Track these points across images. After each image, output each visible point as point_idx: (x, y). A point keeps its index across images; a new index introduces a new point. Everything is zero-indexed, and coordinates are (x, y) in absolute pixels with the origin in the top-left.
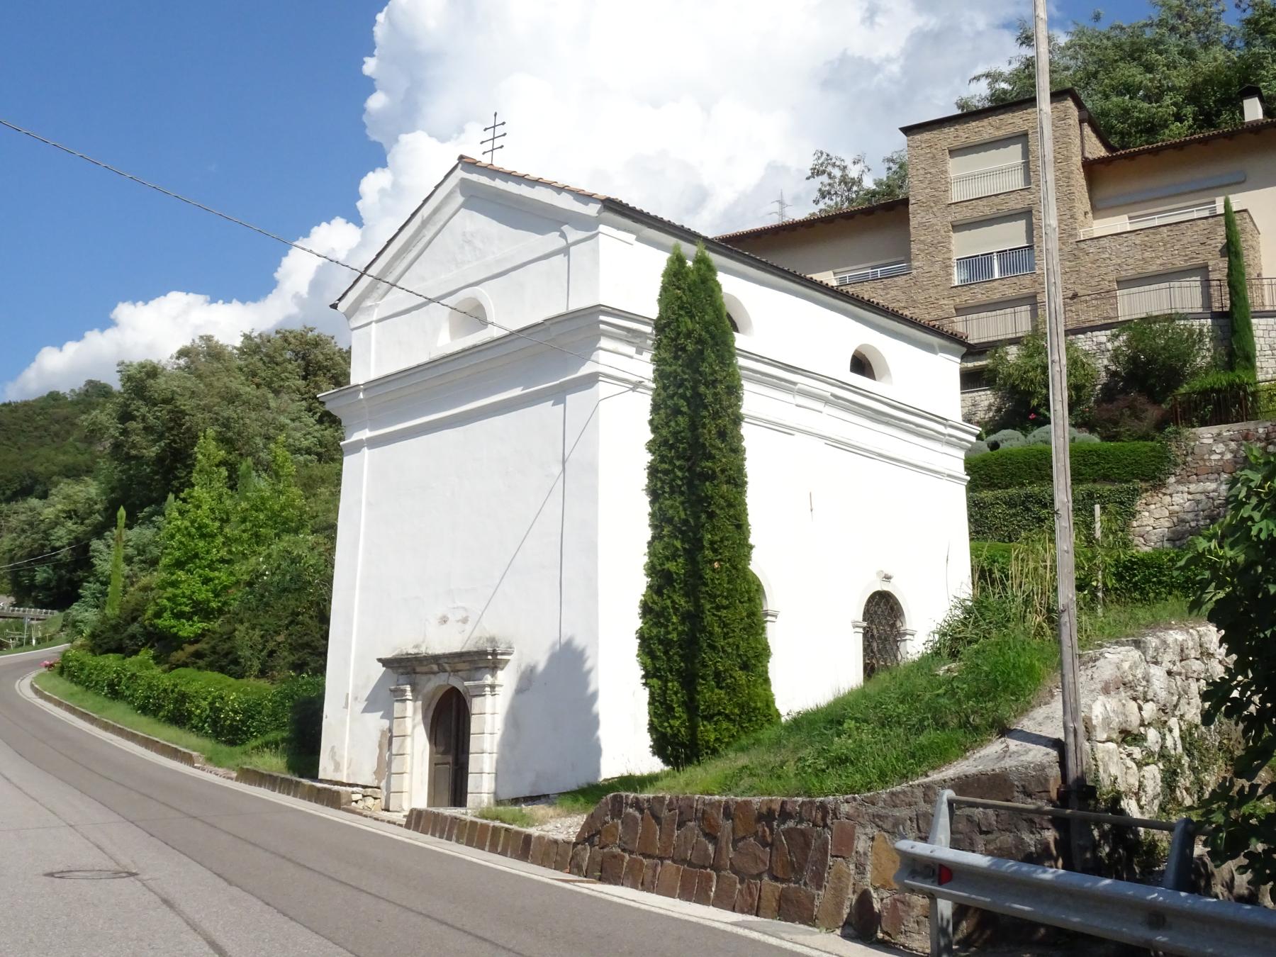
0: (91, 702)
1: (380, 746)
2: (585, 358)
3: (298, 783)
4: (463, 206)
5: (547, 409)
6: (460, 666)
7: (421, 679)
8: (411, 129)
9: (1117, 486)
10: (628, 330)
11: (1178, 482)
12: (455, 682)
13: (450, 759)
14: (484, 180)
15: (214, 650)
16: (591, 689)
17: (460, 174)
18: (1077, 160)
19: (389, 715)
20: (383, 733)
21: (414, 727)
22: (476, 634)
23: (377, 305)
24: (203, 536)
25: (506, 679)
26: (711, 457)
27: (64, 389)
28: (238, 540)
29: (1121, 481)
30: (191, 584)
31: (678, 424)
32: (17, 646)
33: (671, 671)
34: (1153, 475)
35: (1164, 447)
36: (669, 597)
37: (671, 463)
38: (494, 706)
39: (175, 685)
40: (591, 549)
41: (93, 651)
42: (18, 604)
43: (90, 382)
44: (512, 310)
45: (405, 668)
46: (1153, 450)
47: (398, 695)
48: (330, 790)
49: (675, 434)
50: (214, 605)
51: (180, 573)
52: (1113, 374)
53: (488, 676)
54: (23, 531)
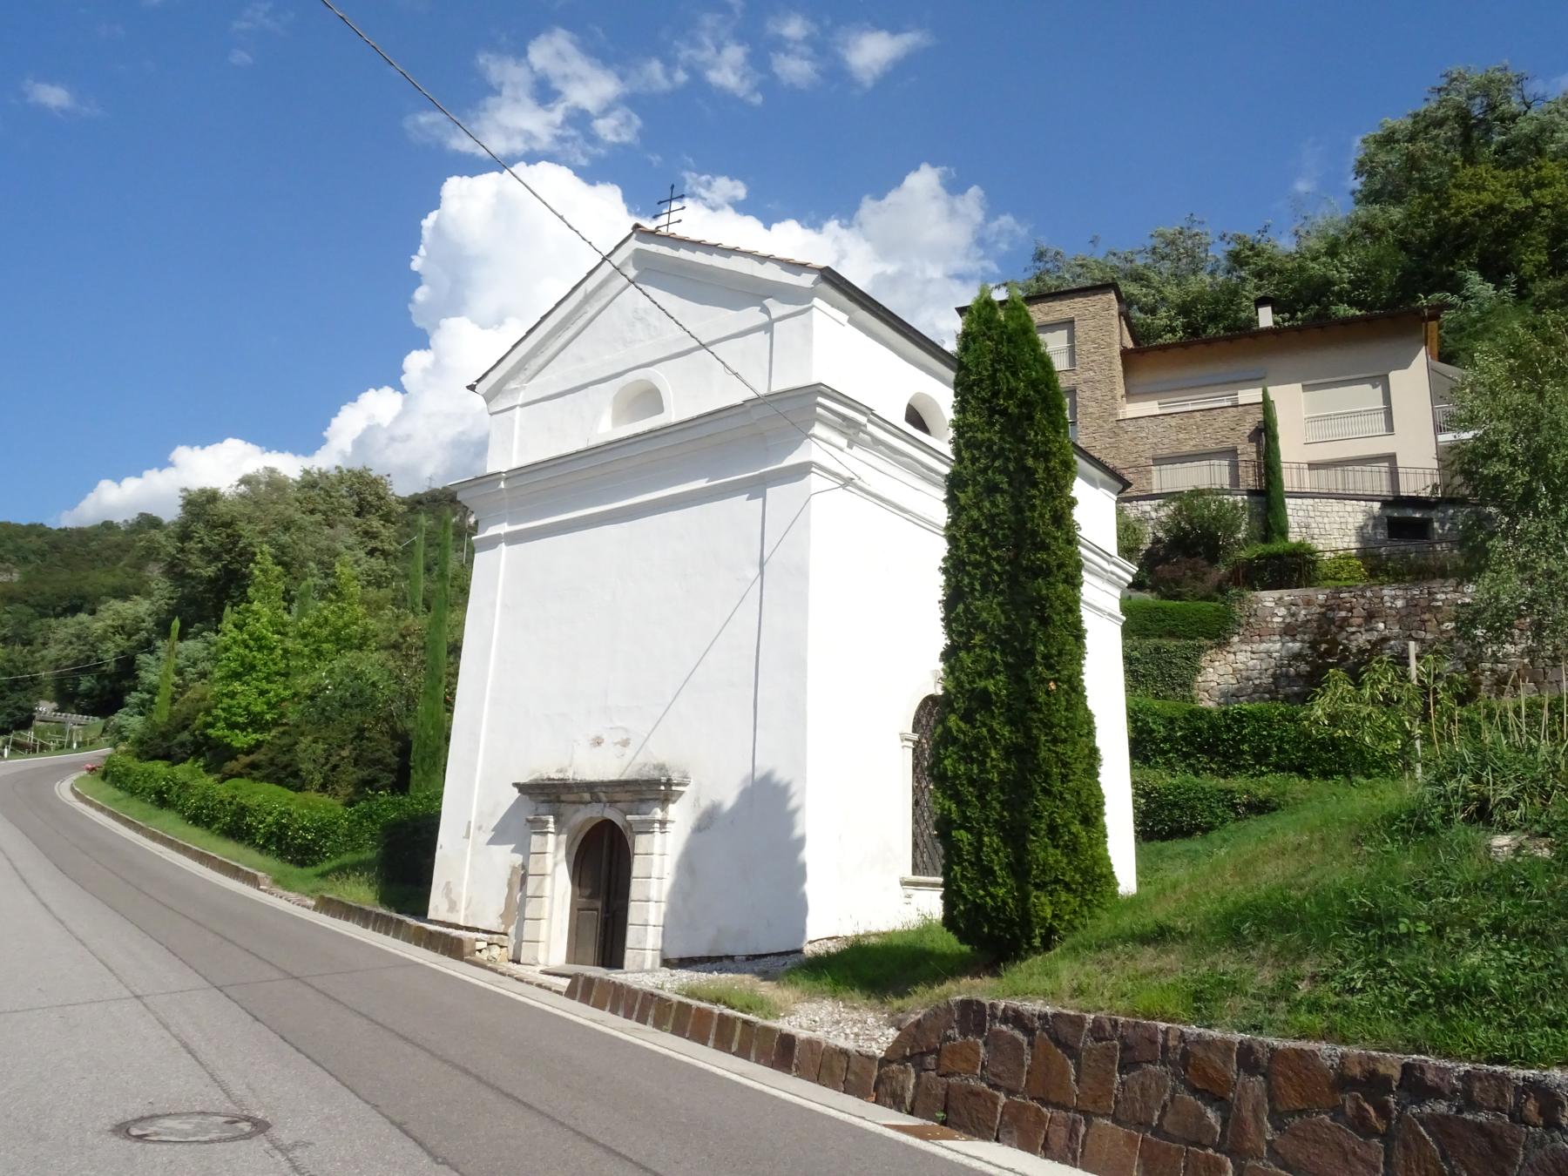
0: (138, 809)
1: (510, 885)
2: (796, 445)
3: (400, 922)
6: (617, 797)
7: (567, 809)
8: (458, 314)
9: (1182, 642)
10: (844, 418)
11: (1241, 641)
12: (612, 814)
13: (599, 904)
14: (665, 250)
15: (272, 762)
16: (798, 832)
17: (634, 244)
18: (1117, 348)
19: (523, 848)
20: (514, 869)
21: (555, 865)
22: (640, 759)
24: (260, 649)
25: (680, 816)
26: (1044, 547)
27: (118, 519)
28: (299, 654)
29: (1186, 638)
30: (247, 695)
31: (994, 504)
32: (57, 749)
33: (986, 822)
34: (1218, 633)
35: (1228, 608)
36: (985, 725)
37: (983, 552)
38: (664, 845)
39: (234, 797)
40: (798, 665)
41: (138, 756)
42: (61, 710)
43: (141, 515)
44: (689, 395)
45: (547, 796)
46: (1217, 609)
47: (538, 827)
48: (447, 936)
49: (991, 519)
50: (268, 717)
51: (236, 684)
52: (1157, 541)
53: (658, 810)
54: (71, 643)
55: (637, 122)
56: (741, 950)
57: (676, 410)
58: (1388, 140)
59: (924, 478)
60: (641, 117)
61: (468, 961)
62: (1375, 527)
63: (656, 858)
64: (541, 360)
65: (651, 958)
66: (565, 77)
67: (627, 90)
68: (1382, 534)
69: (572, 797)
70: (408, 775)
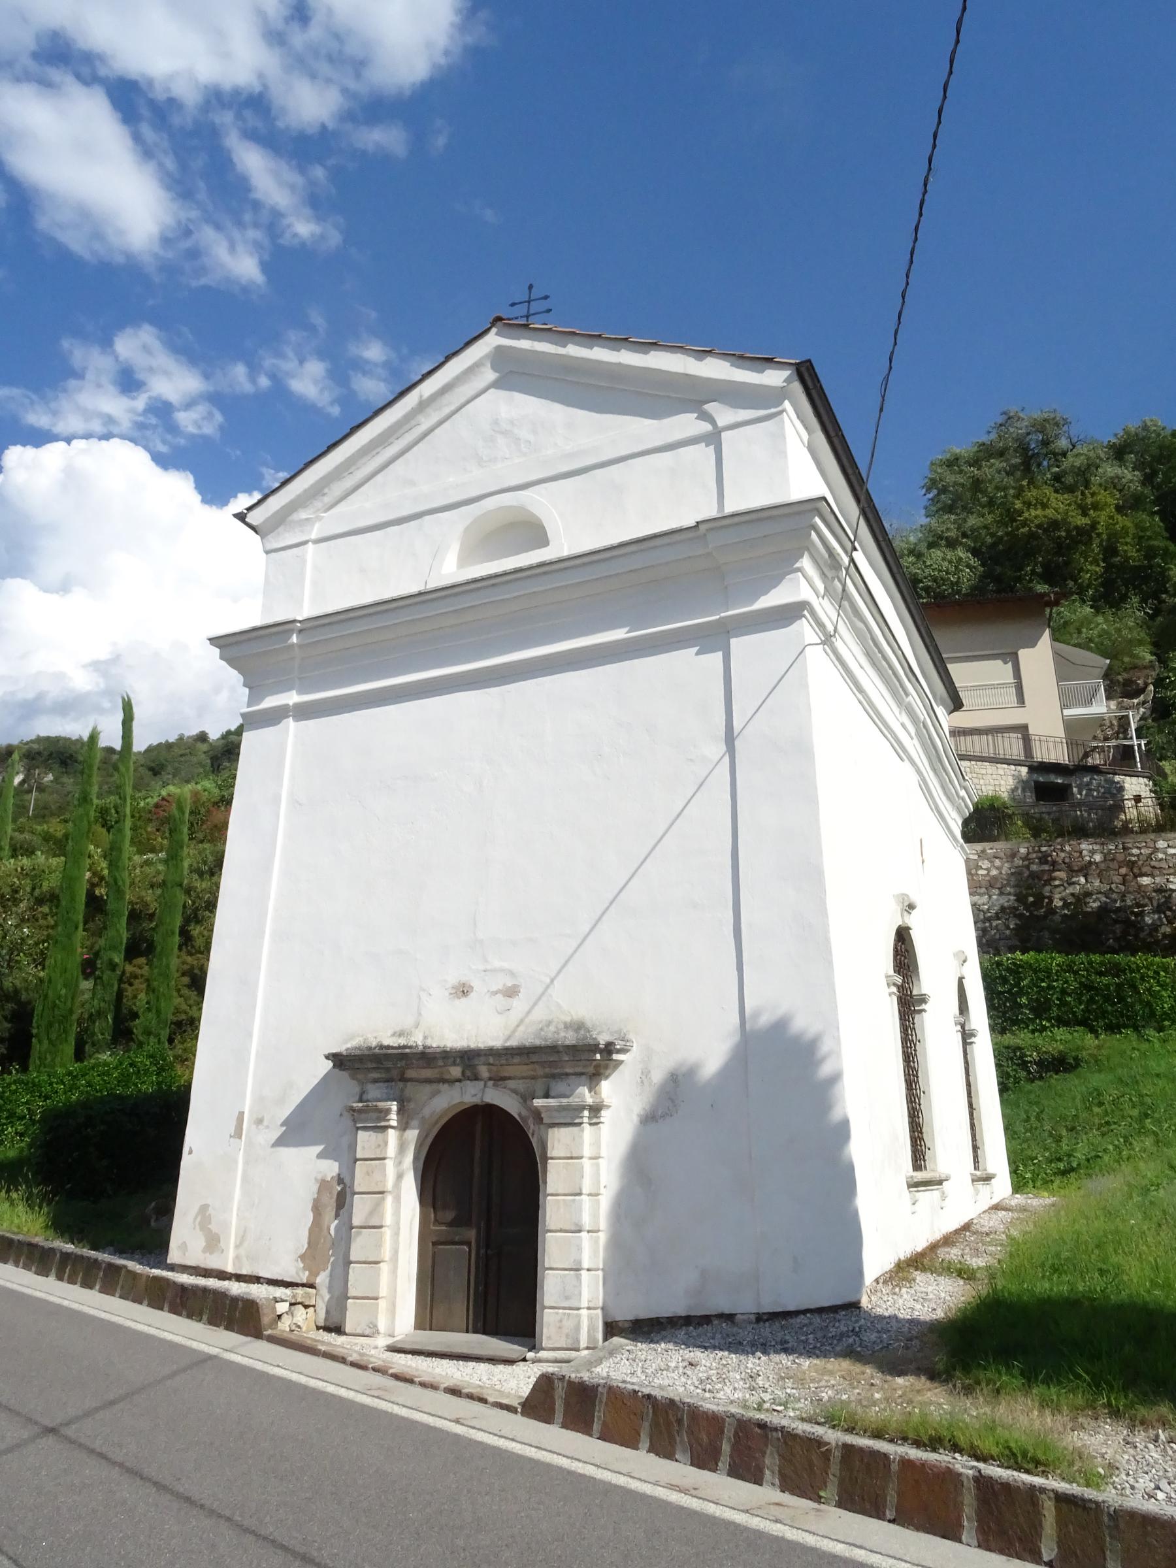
1: (317, 1208)
2: (775, 581)
3: (118, 1269)
4: (496, 385)
5: (685, 659)
6: (508, 1071)
12: (508, 1103)
13: (471, 1234)
16: (836, 1115)
20: (323, 1185)
21: (400, 1176)
23: (319, 519)
25: (621, 1098)
44: (577, 526)
45: (376, 1074)
47: (367, 1117)
48: (220, 1295)
55: (219, 417)
56: (745, 1304)
57: (565, 542)
58: (952, 463)
59: (868, 655)
60: (223, 412)
61: (273, 1340)
62: (1024, 790)
63: (587, 1164)
64: (348, 483)
65: (589, 1324)
66: (151, 370)
67: (211, 389)
68: (1030, 798)
69: (428, 1073)
70: (29, 1045)
